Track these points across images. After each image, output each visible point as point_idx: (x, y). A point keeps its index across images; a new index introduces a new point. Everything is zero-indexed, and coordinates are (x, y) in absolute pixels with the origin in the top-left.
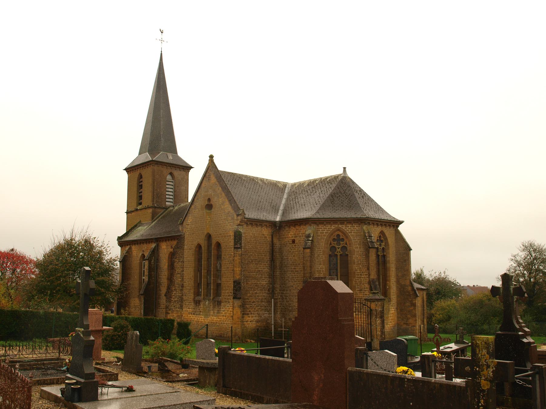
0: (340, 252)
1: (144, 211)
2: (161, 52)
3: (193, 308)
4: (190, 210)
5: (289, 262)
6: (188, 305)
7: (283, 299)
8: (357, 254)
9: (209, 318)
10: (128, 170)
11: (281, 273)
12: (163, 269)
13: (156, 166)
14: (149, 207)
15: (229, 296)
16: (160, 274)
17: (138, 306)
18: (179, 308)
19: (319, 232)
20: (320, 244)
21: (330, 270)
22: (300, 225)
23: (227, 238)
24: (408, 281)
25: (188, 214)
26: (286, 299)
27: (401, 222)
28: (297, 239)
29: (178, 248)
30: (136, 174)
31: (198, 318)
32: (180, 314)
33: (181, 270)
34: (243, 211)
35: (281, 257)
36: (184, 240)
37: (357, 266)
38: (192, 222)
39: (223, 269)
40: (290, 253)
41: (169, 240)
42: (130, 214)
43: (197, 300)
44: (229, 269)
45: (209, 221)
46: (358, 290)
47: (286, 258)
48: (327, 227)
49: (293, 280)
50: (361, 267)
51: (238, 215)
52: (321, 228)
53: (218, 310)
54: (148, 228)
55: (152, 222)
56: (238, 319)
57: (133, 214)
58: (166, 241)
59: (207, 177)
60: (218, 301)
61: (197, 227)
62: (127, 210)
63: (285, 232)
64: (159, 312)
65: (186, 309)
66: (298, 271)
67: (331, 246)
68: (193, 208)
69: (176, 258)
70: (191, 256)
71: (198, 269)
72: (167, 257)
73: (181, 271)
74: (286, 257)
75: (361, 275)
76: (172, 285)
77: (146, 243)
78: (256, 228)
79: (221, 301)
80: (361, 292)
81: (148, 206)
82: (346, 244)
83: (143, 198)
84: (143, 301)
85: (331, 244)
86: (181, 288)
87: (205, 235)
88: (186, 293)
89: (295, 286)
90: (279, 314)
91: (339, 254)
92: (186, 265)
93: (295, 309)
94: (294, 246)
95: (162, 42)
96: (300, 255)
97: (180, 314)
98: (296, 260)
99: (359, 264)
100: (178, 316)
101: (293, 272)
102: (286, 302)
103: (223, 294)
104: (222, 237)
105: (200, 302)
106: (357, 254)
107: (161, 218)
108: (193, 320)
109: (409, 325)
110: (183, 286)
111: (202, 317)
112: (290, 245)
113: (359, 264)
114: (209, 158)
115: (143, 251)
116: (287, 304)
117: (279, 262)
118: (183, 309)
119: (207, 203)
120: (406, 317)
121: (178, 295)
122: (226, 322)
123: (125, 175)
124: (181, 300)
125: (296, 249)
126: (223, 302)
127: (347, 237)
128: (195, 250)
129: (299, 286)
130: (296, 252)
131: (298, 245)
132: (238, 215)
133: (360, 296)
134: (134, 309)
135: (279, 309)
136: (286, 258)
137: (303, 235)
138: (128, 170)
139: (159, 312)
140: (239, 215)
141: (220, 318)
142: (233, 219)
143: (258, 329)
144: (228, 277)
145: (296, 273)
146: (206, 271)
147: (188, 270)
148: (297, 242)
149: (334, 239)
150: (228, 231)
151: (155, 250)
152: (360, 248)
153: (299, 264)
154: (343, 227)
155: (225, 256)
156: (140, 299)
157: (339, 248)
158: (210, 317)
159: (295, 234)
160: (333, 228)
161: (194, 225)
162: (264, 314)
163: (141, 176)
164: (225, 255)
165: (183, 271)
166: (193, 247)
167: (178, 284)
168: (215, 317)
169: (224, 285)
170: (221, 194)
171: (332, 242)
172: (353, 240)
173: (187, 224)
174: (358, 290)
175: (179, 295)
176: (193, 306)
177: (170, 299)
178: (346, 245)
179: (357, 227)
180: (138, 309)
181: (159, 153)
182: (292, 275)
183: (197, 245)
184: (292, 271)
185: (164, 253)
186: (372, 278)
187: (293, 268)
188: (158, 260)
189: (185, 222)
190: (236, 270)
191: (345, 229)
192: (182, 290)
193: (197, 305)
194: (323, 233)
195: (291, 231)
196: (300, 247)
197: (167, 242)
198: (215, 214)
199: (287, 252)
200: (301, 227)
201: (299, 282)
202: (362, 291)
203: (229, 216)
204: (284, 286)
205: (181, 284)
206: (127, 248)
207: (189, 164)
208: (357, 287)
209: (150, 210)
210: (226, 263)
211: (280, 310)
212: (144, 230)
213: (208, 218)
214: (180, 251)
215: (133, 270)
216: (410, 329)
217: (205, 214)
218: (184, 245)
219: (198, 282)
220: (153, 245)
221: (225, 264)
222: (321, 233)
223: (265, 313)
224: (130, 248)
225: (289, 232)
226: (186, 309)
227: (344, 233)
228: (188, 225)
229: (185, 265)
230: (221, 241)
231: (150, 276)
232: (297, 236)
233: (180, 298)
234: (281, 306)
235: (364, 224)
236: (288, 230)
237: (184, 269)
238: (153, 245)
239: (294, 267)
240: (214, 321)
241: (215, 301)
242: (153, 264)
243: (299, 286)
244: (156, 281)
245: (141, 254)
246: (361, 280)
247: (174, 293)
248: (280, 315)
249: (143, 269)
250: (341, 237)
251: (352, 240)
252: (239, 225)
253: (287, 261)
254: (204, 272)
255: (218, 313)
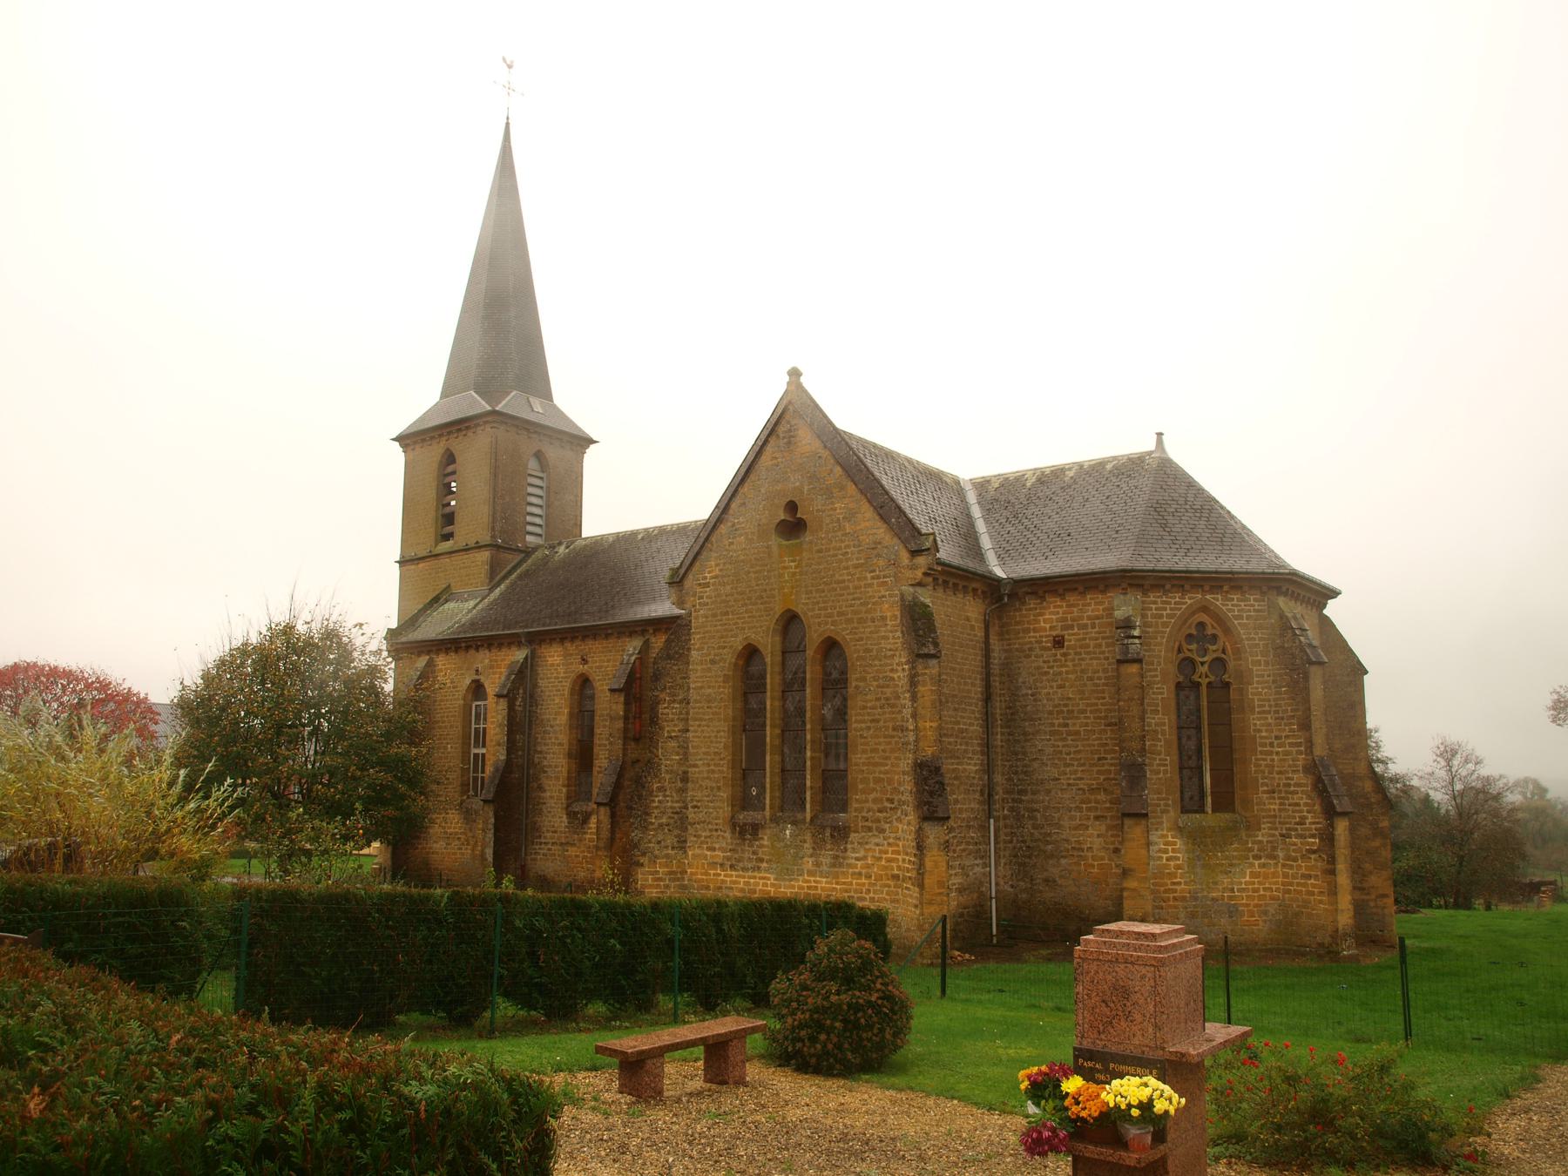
0: (1207, 676)
1: (457, 558)
2: (508, 118)
3: (730, 847)
4: (713, 539)
5: (1044, 706)
6: (706, 837)
7: (1019, 818)
8: (1258, 682)
9: (798, 880)
10: (405, 440)
11: (1011, 737)
12: (552, 726)
13: (503, 428)
14: (479, 547)
15: (880, 811)
16: (539, 740)
17: (456, 833)
18: (673, 848)
19: (1149, 613)
20: (1154, 650)
21: (1180, 728)
22: (1083, 594)
23: (869, 626)
24: (1363, 764)
25: (704, 553)
26: (1030, 818)
27: (1333, 593)
28: (1073, 634)
29: (669, 657)
30: (436, 451)
31: (752, 881)
32: (679, 867)
33: (681, 727)
34: (935, 540)
35: (1009, 689)
36: (689, 634)
37: (1259, 719)
38: (723, 576)
39: (854, 725)
40: (1045, 678)
41: (573, 639)
42: (413, 567)
43: (745, 824)
44: (881, 723)
45: (794, 574)
46: (1264, 792)
47: (1030, 692)
48: (1171, 598)
49: (1059, 759)
50: (1270, 721)
51: (915, 553)
52: (1155, 603)
53: (836, 857)
54: (480, 606)
55: (491, 590)
56: (938, 888)
57: (421, 565)
58: (562, 640)
59: (781, 435)
60: (834, 828)
61: (742, 593)
62: (402, 556)
63: (1024, 612)
64: (539, 854)
65: (697, 851)
66: (1077, 733)
67: (1182, 656)
68: (723, 532)
69: (662, 691)
70: (717, 684)
71: (744, 726)
72: (567, 689)
73: (679, 731)
74: (1031, 688)
75: (1271, 745)
76: (649, 773)
77: (490, 647)
78: (953, 598)
79: (849, 827)
80: (1274, 798)
81: (477, 542)
82: (1224, 652)
83: (457, 518)
84: (493, 820)
85: (1179, 651)
86: (679, 784)
87: (777, 617)
88: (698, 801)
89: (1069, 779)
90: (1005, 864)
91: (1204, 681)
92: (697, 713)
93: (1068, 851)
94: (1059, 657)
95: (511, 91)
96: (1085, 685)
97: (679, 867)
98: (1069, 699)
99: (1264, 712)
100: (671, 873)
101: (1057, 737)
102: (1034, 828)
103: (855, 805)
104: (849, 621)
105: (757, 830)
106: (1258, 682)
107: (520, 577)
108: (728, 885)
109: (1368, 894)
110: (685, 779)
111: (769, 879)
112: (1046, 654)
113: (1264, 712)
114: (787, 378)
115: (477, 671)
116: (1036, 834)
117: (1004, 705)
118: (685, 852)
119: (783, 518)
120: (1359, 868)
121: (671, 807)
122: (872, 895)
123: (397, 456)
124: (681, 822)
125: (1070, 664)
126: (855, 832)
127: (1227, 631)
128: (736, 665)
129: (1082, 779)
130: (1067, 673)
131: (1076, 654)
132: (915, 553)
133: (1270, 810)
134: (442, 844)
135: (1005, 850)
136: (1030, 692)
137: (1097, 621)
138: (408, 441)
139: (539, 854)
140: (923, 550)
141: (844, 883)
142: (895, 564)
143: (962, 915)
144: (875, 750)
145: (1070, 738)
146: (778, 731)
147: (708, 726)
148: (1073, 642)
149: (1190, 635)
150: (874, 604)
151: (527, 667)
152: (1267, 663)
153: (1083, 712)
154: (1218, 600)
155: (861, 684)
156: (468, 815)
157: (1202, 663)
158: (801, 878)
159: (1064, 620)
160: (1189, 602)
161: (728, 587)
162: (973, 866)
163: (450, 458)
164: (864, 679)
165: (688, 731)
166: (729, 657)
167: (671, 772)
168: (820, 877)
169: (860, 777)
170: (842, 488)
171: (1185, 646)
172: (1248, 639)
173: (700, 584)
174: (1264, 792)
175: (675, 808)
176: (729, 841)
177: (645, 820)
178: (1223, 656)
179: (1255, 600)
180: (457, 842)
181: (508, 393)
182: (1054, 746)
183: (744, 648)
184: (1052, 733)
185: (557, 678)
186: (1318, 753)
187: (1056, 722)
188: (532, 699)
189: (691, 577)
190: (925, 729)
191: (1223, 605)
192: (683, 790)
193: (745, 839)
194: (1161, 616)
195: (1047, 612)
196: (1083, 659)
197: (568, 644)
198: (820, 551)
199: (1033, 675)
200: (1088, 597)
201: (1083, 765)
202: (1276, 795)
203: (878, 556)
204: (1023, 780)
205: (680, 772)
206: (422, 662)
207: (580, 430)
208: (1261, 781)
209: (485, 555)
210: (869, 705)
211: (1007, 853)
212: (470, 611)
213: (787, 564)
214: (675, 668)
215: (440, 728)
216: (1372, 904)
217: (775, 549)
218: (689, 649)
219: (744, 767)
220: (520, 655)
221: (865, 708)
222: (1155, 616)
223: (976, 862)
224: (430, 664)
225: (1041, 614)
226: (697, 851)
227: (1220, 620)
228: (707, 585)
229: (691, 711)
230: (844, 634)
231: (511, 746)
232: (1073, 626)
233: (676, 816)
234: (1011, 842)
235: (1275, 593)
236: (1036, 609)
237: (691, 723)
238: (520, 655)
239: (1061, 721)
240: (819, 892)
241: (823, 828)
242: (520, 709)
243: (1082, 779)
244: (528, 760)
245: (468, 681)
246: (1273, 760)
247: (657, 799)
248: (1007, 867)
249: (473, 726)
250: (1210, 631)
251: (1242, 639)
252: (920, 584)
253: (1035, 700)
254: (770, 734)
255: (834, 865)
